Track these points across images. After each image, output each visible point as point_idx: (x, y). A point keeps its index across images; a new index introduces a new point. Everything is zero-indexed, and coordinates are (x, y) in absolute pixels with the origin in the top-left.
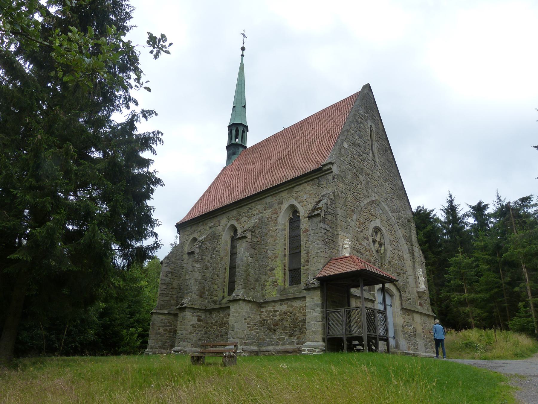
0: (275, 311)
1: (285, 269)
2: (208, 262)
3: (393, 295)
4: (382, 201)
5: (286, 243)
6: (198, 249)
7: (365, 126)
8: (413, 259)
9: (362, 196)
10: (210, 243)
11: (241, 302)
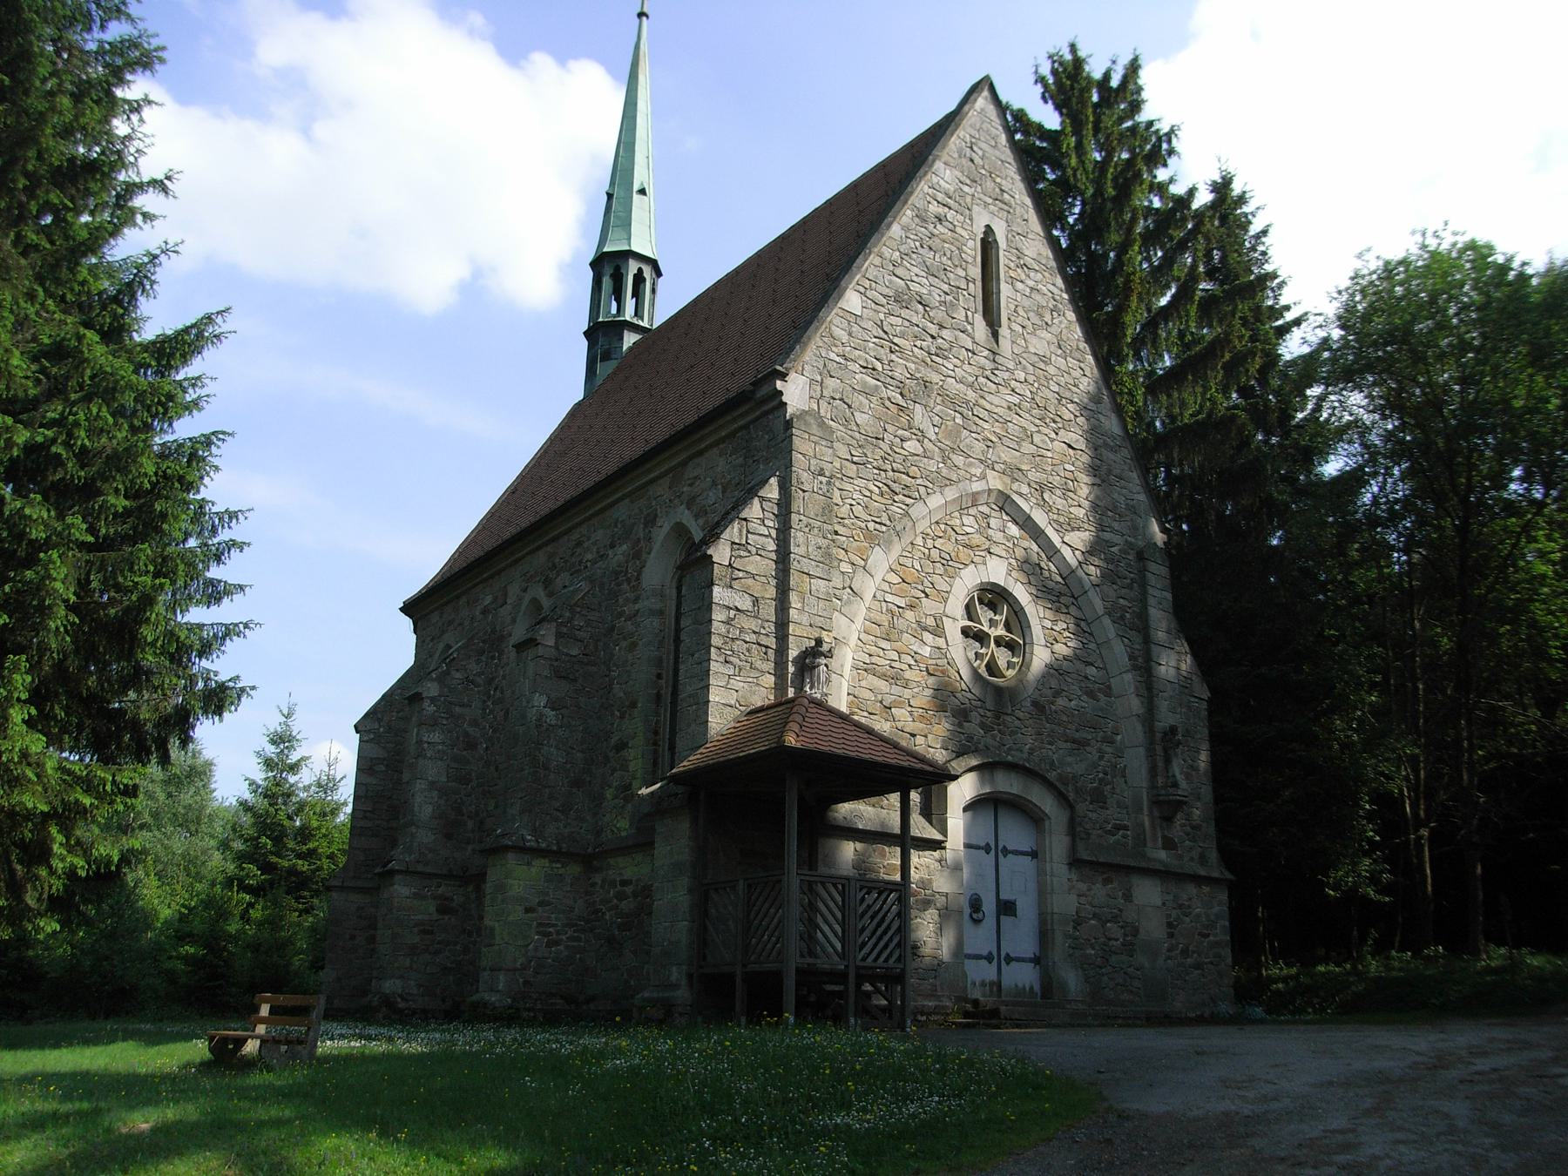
0: (624, 883)
1: (655, 744)
2: (474, 723)
3: (1043, 820)
4: (1021, 494)
5: (665, 656)
6: (436, 684)
7: (959, 230)
8: (1150, 688)
9: (919, 481)
10: (478, 662)
11: (510, 856)
